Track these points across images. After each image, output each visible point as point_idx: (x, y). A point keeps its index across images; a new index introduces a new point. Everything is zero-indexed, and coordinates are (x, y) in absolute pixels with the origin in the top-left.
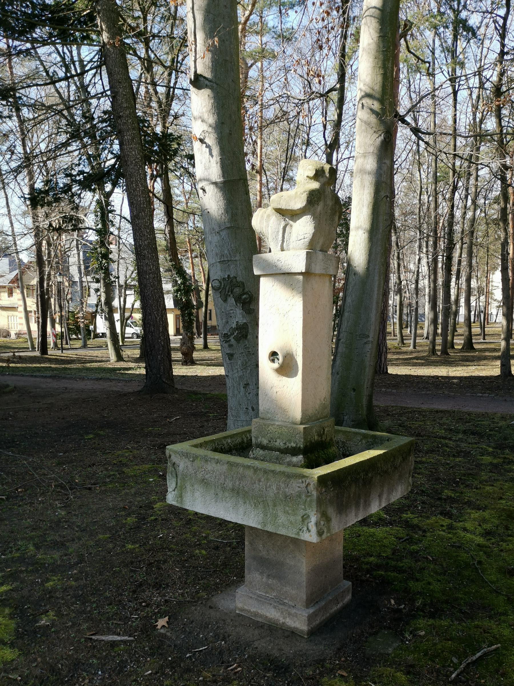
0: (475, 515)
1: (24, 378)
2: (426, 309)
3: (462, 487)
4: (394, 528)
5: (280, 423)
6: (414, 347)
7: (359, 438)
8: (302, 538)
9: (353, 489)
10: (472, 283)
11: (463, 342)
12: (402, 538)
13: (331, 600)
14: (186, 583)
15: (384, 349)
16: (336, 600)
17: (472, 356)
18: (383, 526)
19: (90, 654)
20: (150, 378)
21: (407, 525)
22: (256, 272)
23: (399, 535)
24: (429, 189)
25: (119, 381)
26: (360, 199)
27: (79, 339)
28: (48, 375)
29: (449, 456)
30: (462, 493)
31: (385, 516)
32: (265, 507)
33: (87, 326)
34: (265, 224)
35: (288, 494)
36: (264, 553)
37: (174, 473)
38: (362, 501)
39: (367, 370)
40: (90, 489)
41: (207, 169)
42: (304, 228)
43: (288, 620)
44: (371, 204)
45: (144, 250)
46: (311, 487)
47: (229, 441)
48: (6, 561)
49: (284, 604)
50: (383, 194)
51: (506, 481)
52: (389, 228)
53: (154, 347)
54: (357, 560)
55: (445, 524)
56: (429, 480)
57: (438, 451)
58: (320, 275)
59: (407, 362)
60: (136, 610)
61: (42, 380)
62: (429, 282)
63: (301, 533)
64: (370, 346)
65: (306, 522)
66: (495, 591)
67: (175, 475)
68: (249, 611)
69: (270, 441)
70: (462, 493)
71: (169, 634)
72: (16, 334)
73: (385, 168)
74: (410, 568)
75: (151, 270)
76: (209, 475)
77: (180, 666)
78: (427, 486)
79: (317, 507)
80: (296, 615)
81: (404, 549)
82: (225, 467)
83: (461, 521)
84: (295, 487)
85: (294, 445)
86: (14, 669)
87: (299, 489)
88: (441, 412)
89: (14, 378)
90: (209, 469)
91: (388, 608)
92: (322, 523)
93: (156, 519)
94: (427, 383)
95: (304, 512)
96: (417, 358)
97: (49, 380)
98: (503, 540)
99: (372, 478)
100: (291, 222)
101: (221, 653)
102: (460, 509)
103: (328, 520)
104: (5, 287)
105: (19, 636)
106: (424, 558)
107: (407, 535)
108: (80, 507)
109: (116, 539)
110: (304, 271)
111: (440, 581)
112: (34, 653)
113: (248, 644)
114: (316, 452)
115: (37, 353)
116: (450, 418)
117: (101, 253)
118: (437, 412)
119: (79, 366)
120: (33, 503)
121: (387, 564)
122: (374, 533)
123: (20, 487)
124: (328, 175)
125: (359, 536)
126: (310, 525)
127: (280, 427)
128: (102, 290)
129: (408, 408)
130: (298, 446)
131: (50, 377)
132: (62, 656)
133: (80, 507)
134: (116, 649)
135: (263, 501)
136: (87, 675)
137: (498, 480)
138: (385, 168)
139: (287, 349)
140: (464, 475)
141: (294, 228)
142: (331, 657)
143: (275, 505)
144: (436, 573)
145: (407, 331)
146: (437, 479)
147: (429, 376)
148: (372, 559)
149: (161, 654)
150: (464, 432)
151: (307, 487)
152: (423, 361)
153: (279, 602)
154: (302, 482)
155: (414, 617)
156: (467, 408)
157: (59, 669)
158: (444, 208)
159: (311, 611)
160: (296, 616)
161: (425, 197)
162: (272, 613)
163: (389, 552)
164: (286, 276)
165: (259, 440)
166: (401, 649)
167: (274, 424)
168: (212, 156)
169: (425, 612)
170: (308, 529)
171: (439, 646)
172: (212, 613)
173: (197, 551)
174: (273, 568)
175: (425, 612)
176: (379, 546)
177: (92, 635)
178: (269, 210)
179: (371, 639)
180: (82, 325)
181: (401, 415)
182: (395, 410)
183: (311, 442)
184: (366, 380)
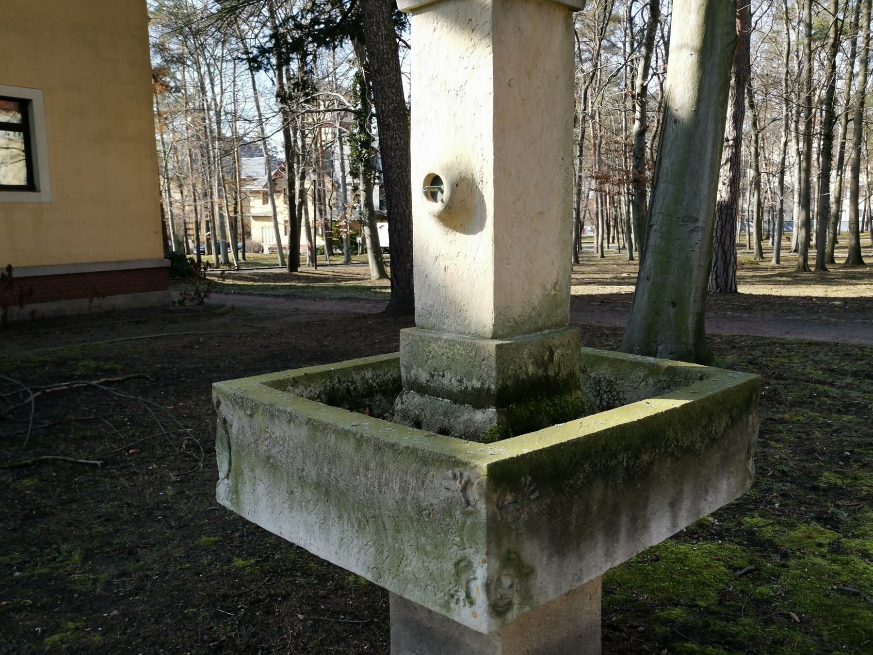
2: (795, 214)
3: (855, 466)
4: (727, 545)
6: (778, 261)
7: (641, 374)
8: (456, 619)
9: (598, 492)
10: (860, 179)
11: (847, 255)
12: (741, 569)
15: (733, 259)
17: (861, 273)
18: (705, 539)
20: (397, 294)
21: (752, 539)
24: (801, 53)
25: (368, 301)
27: (343, 254)
28: (281, 294)
29: (830, 411)
30: (856, 478)
32: (377, 532)
33: (353, 237)
35: (424, 504)
37: (224, 440)
38: (624, 519)
39: (695, 273)
44: (704, 8)
45: (388, 117)
46: (474, 493)
47: (369, 375)
52: (731, 46)
53: (402, 251)
54: (647, 612)
56: (795, 453)
59: (766, 280)
61: (273, 300)
62: (800, 171)
63: (453, 605)
64: (700, 235)
65: (464, 578)
67: (226, 445)
69: (432, 376)
70: (856, 478)
72: (269, 249)
74: (752, 638)
75: (397, 145)
78: (791, 464)
79: (489, 543)
81: (742, 592)
82: (304, 431)
83: (858, 537)
84: (441, 487)
85: (477, 384)
87: (449, 494)
88: (817, 344)
89: (239, 297)
90: (277, 434)
94: (795, 305)
95: (460, 554)
96: (781, 275)
97: (281, 300)
99: (652, 463)
102: (854, 511)
103: (524, 573)
104: (258, 192)
106: (782, 615)
107: (751, 562)
114: (524, 400)
115: (285, 271)
116: (830, 353)
119: (331, 284)
121: (706, 625)
122: (686, 555)
125: (658, 559)
127: (451, 343)
128: (361, 187)
129: (765, 338)
130: (486, 386)
131: (284, 296)
135: (374, 517)
139: (462, 168)
140: (859, 445)
143: (398, 531)
145: (768, 244)
146: (811, 451)
147: (798, 297)
148: (676, 612)
150: (855, 374)
151: (464, 489)
152: (789, 279)
154: (455, 477)
158: (820, 76)
161: (794, 64)
165: (413, 372)
167: (439, 339)
170: (468, 596)
180: (344, 236)
181: (753, 348)
182: (745, 341)
183: (516, 378)
184: (694, 290)
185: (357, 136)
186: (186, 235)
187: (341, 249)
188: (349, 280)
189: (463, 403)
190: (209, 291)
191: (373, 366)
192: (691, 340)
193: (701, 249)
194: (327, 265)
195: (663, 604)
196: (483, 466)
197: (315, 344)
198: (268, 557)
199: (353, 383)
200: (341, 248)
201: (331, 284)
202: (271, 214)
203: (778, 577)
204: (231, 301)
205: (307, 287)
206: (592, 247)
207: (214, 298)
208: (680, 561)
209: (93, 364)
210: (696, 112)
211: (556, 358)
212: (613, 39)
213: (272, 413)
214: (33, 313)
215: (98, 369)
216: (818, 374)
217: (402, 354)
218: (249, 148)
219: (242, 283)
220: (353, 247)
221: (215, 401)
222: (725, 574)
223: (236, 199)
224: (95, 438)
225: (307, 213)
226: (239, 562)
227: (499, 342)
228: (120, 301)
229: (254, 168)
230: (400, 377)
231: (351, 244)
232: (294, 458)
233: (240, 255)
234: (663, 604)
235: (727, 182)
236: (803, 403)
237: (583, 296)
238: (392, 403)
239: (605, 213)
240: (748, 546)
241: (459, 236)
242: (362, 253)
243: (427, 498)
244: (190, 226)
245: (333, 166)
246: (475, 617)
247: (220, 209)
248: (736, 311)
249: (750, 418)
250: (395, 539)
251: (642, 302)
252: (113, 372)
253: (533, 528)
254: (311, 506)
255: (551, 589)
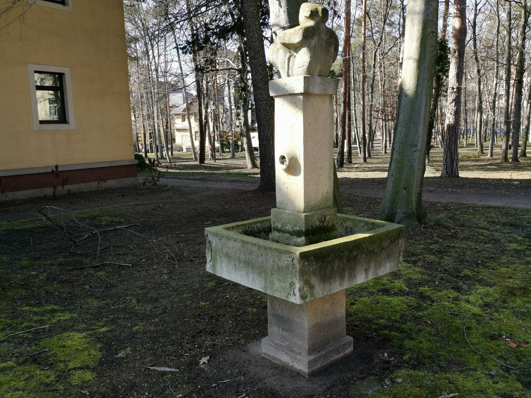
0: (482, 290)
1: (181, 181)
5: (289, 212)
6: (492, 156)
7: (362, 225)
9: (337, 263)
13: (332, 351)
14: (233, 332)
15: (456, 157)
16: (337, 351)
18: (401, 296)
19: (145, 380)
20: (263, 180)
21: (422, 296)
22: (272, 94)
23: (411, 304)
26: (411, 35)
27: (230, 152)
31: (406, 288)
33: (236, 143)
34: (275, 56)
35: (280, 266)
36: (279, 312)
37: (210, 249)
39: (416, 173)
40: (192, 261)
41: (277, 16)
42: (303, 57)
43: (295, 364)
44: (420, 39)
45: (259, 82)
46: (295, 261)
47: (259, 225)
48: (113, 310)
49: (293, 351)
50: (429, 30)
51: (521, 264)
53: (266, 156)
55: (452, 296)
57: (473, 239)
58: (320, 95)
59: (482, 168)
60: (190, 350)
65: (292, 288)
66: (473, 351)
68: (270, 356)
71: (206, 369)
72: (186, 149)
73: (432, 9)
76: (230, 251)
77: (205, 393)
80: (300, 360)
82: (240, 244)
85: (299, 229)
86: (88, 387)
87: (288, 262)
88: (493, 207)
89: (174, 180)
91: (380, 360)
92: (306, 289)
93: (229, 284)
94: (490, 184)
97: (198, 182)
98: (497, 311)
100: (295, 54)
101: (239, 385)
104: (179, 115)
105: (101, 363)
106: (425, 322)
108: (180, 274)
109: (194, 298)
110: (302, 92)
111: (430, 341)
112: (106, 376)
113: (260, 380)
114: (313, 234)
115: (197, 163)
117: (241, 87)
118: (489, 207)
119: (225, 171)
120: (149, 270)
121: (393, 325)
122: (390, 301)
123: (144, 258)
124: (321, 15)
125: (378, 303)
126: (295, 290)
127: (289, 214)
131: (199, 179)
132: (124, 380)
133: (180, 274)
134: (164, 377)
136: (137, 395)
137: (514, 263)
138: (431, 9)
139: (293, 154)
140: (487, 258)
141: (296, 58)
142: (320, 394)
143: (272, 275)
144: (430, 334)
149: (195, 383)
150: (504, 224)
151: (292, 260)
152: (495, 167)
153: (290, 350)
155: (399, 367)
156: (518, 205)
157: (119, 389)
159: (312, 357)
160: (300, 361)
162: (285, 358)
163: (399, 315)
164: (291, 97)
165: (276, 224)
166: (379, 392)
168: (281, 7)
169: (409, 365)
170: (294, 293)
171: (408, 392)
172: (244, 355)
173: (250, 309)
174: (286, 323)
175: (409, 365)
176: (392, 311)
177: (151, 366)
178: (279, 46)
179: (358, 383)
183: (312, 226)
184: (416, 181)
185: (239, 84)
186: (138, 140)
187: (229, 148)
188: (235, 168)
189: (293, 235)
190: (159, 177)
191: (261, 222)
192: (414, 206)
193: (419, 160)
194: (221, 159)
195: (377, 318)
196: (298, 253)
197: (220, 208)
198: (214, 302)
199: (253, 228)
200: (229, 148)
201: (225, 171)
202: (188, 128)
203: (427, 309)
204: (171, 182)
205: (212, 173)
206: (380, 146)
207: (162, 181)
208: (388, 303)
209: (109, 219)
210: (416, 92)
211: (327, 219)
212: (392, 20)
213: (228, 238)
214: (69, 191)
215: (112, 221)
216: (483, 224)
217: (271, 217)
218: (175, 88)
219: (173, 171)
220: (237, 148)
221: (206, 234)
222: (406, 308)
223: (167, 120)
224: (124, 255)
225: (209, 128)
226: (202, 303)
227: (306, 214)
228: (112, 183)
229: (177, 99)
230: (271, 226)
231: (235, 146)
232: (236, 253)
233: (170, 153)
234: (377, 318)
235: (453, 113)
236: (468, 239)
237: (369, 179)
238: (268, 236)
239: (387, 127)
240: (418, 298)
241: (292, 177)
242: (242, 151)
243: (281, 264)
244: (140, 135)
245: (224, 100)
246: (296, 299)
247: (159, 126)
248: (454, 188)
249: (400, 241)
250: (271, 277)
251: (390, 186)
252: (120, 223)
253: (314, 273)
254: (242, 269)
255: (320, 293)
